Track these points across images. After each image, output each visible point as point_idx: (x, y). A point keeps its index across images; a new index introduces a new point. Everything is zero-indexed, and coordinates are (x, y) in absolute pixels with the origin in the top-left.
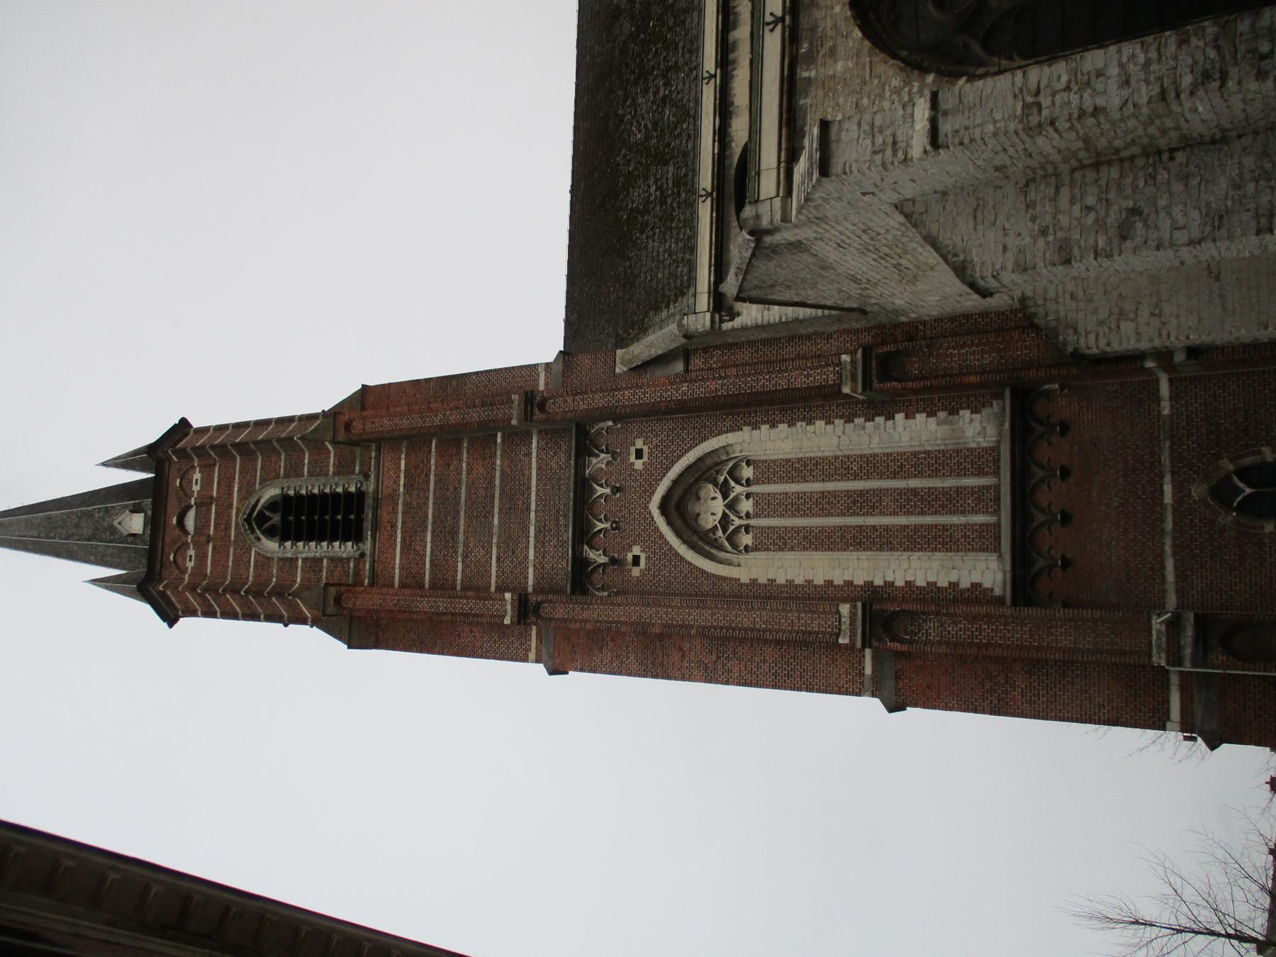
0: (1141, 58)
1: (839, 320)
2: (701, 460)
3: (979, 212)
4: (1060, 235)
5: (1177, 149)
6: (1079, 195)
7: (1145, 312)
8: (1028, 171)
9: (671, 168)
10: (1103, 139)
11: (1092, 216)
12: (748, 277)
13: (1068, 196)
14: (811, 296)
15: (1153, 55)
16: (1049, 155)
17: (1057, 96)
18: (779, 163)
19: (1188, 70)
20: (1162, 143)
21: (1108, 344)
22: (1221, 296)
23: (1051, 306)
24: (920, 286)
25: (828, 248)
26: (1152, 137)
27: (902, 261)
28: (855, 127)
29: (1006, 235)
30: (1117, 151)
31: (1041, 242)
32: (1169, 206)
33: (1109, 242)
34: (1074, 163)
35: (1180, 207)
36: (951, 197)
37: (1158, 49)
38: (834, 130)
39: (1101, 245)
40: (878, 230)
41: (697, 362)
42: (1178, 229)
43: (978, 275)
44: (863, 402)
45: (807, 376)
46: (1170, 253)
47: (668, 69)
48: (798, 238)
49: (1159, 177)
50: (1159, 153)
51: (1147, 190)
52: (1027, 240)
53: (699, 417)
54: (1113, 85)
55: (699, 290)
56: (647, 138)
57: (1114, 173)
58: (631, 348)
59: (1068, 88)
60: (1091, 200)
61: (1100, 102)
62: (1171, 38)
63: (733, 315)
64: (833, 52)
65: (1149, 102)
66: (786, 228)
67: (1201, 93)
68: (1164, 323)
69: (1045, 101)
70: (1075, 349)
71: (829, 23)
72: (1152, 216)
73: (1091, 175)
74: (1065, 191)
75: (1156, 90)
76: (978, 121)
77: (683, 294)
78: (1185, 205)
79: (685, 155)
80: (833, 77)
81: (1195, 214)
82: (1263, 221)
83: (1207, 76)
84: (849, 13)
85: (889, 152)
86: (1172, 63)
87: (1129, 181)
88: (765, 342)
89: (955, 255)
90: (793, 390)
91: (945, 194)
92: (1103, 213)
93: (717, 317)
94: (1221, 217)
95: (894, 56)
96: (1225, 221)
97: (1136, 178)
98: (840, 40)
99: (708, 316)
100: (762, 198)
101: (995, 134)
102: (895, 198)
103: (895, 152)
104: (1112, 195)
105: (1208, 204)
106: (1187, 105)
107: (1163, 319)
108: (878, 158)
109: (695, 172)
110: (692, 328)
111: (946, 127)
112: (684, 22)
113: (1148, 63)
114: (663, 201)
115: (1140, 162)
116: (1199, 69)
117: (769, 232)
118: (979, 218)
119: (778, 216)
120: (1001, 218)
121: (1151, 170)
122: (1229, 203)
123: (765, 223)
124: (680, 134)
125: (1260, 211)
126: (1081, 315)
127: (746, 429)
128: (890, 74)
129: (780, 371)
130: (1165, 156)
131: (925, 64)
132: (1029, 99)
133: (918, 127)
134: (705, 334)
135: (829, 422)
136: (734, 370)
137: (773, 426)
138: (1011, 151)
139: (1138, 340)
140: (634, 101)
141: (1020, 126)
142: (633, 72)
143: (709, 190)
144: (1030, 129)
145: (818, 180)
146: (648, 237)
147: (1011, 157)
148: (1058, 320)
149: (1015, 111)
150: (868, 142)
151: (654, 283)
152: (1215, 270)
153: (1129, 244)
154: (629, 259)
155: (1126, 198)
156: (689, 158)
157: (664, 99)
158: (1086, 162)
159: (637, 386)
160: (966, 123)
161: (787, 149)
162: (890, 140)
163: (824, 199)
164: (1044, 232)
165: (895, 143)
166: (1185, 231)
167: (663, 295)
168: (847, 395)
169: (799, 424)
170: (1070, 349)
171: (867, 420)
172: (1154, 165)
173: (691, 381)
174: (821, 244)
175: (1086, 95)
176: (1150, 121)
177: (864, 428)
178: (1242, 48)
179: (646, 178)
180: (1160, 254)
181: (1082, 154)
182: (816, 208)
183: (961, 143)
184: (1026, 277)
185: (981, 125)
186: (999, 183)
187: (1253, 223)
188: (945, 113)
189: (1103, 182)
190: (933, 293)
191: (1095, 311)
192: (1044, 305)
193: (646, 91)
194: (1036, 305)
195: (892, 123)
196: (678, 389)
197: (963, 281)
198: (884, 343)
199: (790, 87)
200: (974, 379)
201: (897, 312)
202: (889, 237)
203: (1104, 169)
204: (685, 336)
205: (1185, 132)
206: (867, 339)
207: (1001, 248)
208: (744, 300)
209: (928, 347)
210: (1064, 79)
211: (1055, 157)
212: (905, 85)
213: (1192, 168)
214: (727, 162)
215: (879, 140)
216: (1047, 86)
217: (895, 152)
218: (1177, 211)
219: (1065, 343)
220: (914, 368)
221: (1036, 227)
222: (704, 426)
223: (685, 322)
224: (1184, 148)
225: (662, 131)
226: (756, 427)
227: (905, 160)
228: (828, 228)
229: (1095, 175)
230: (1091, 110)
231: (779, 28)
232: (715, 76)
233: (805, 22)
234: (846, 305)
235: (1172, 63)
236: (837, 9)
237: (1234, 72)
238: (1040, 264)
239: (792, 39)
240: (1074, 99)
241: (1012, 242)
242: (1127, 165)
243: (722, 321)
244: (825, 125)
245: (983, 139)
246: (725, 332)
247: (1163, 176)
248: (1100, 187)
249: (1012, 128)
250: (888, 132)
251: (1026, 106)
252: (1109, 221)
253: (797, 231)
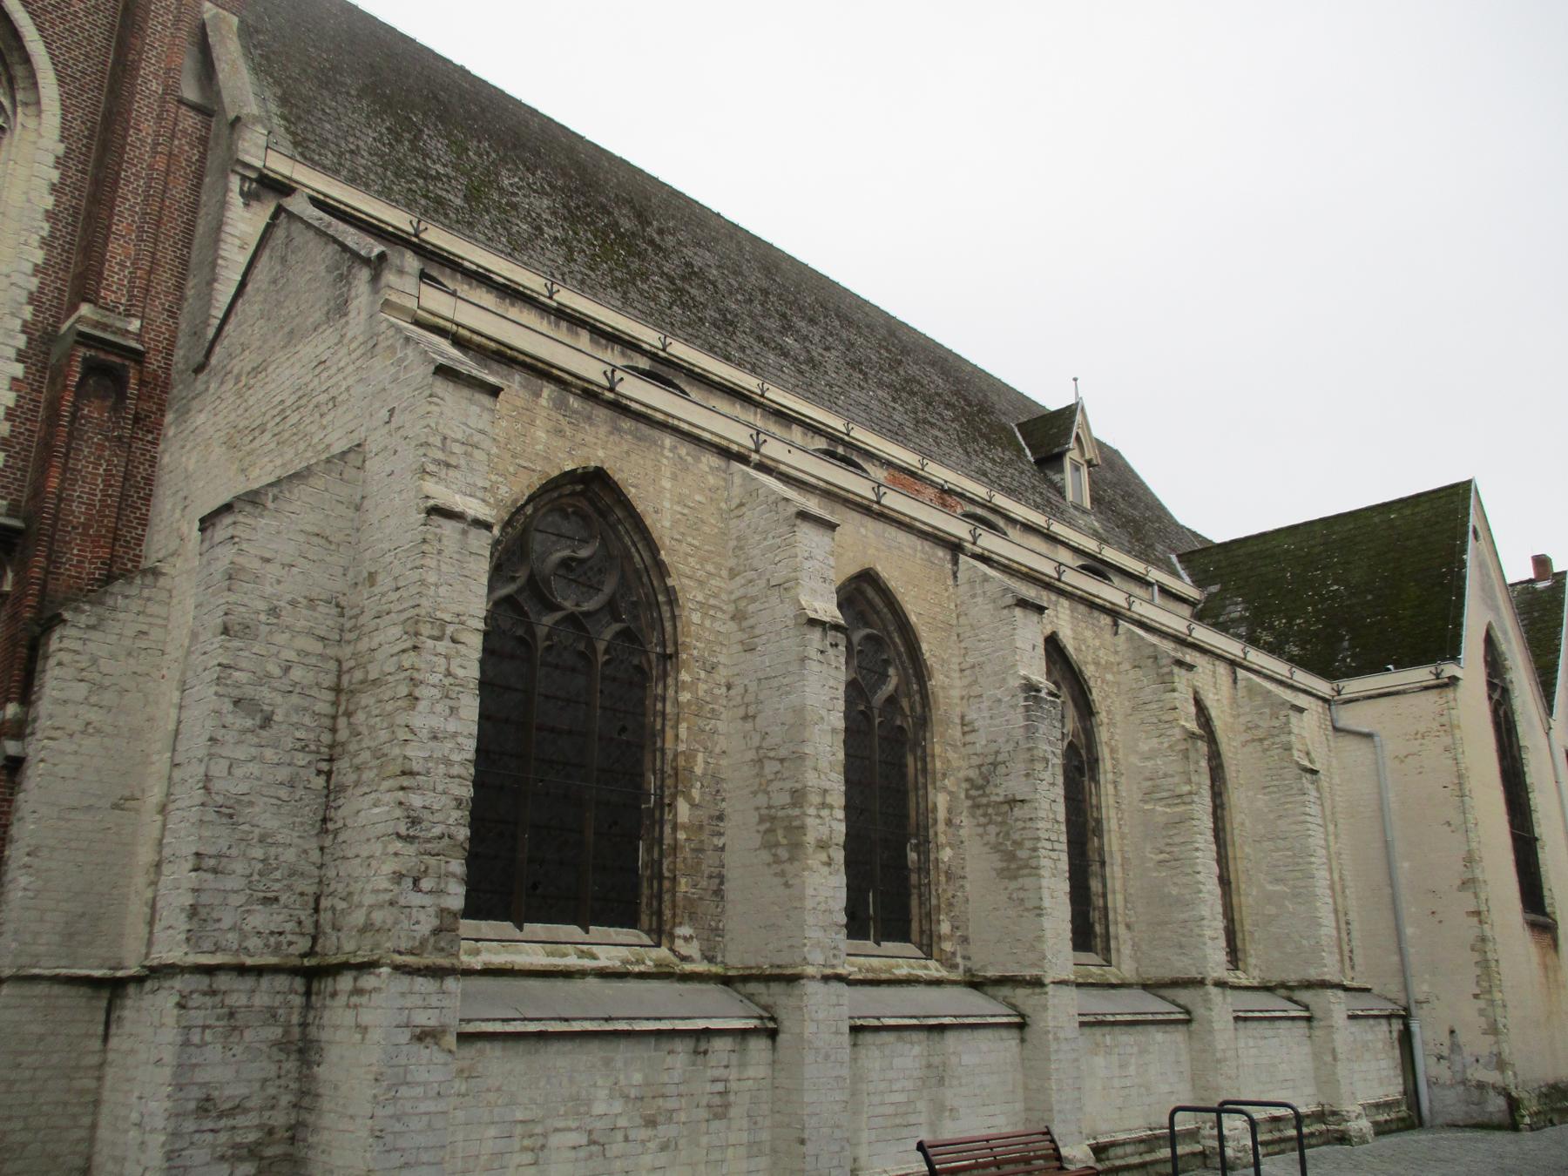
0: (456, 757)
1: (196, 334)
2: (26, 59)
3: (322, 542)
4: (264, 629)
5: (328, 781)
6: (307, 661)
7: (94, 715)
8: (356, 611)
9: (458, 202)
10: (372, 701)
11: (277, 672)
12: (311, 234)
13: (310, 649)
14: (249, 308)
15: (456, 770)
16: (371, 638)
17: (443, 661)
18: (458, 325)
19: (427, 804)
20: (343, 765)
21: (60, 664)
22: (90, 807)
23: (135, 606)
24: (218, 450)
25: (322, 347)
26: (356, 755)
27: (267, 436)
28: (481, 426)
29: (283, 565)
30: (348, 714)
31: (262, 605)
32: (262, 760)
33: (238, 685)
34: (346, 666)
35: (257, 773)
36: (350, 513)
37: (459, 777)
38: (486, 400)
39: (237, 674)
40: (329, 417)
41: (189, 121)
42: (230, 767)
43: (240, 518)
44: (56, 328)
45: (122, 264)
46: (201, 753)
47: (571, 250)
48: (353, 314)
49: (301, 755)
50: (331, 760)
51: (290, 739)
52: (268, 590)
53: (100, 88)
54: (436, 722)
55: (299, 167)
56: (501, 189)
57: (323, 707)
58: (235, 39)
59: (448, 674)
60: (297, 674)
61: (422, 706)
62: (467, 792)
63: (249, 197)
64: (559, 432)
65: (405, 757)
66: (374, 303)
67: (398, 813)
68: (71, 736)
69: (442, 646)
70: (64, 621)
71: (590, 439)
72: (256, 740)
73: (329, 680)
74: (318, 647)
75: (416, 767)
76: (444, 568)
77: (296, 144)
78: (258, 779)
79: (470, 225)
80: (532, 423)
81: (243, 788)
82: (212, 862)
83: (414, 822)
84: (593, 464)
85: (440, 456)
86: (440, 788)
87: (307, 720)
88: (190, 228)
89: (275, 498)
90: (107, 238)
91: (358, 508)
92: (276, 684)
93: (253, 175)
94: (231, 816)
95: (531, 499)
96: (224, 820)
97: (308, 729)
98: (568, 444)
99: (259, 164)
100: (423, 286)
101: (423, 582)
102: (372, 447)
103: (438, 462)
104: (295, 699)
105: (251, 804)
106: (387, 797)
107: (78, 736)
108: (437, 441)
109: (449, 228)
110: (248, 135)
111: (449, 528)
112: (614, 287)
113: (448, 762)
114: (421, 173)
115: (326, 738)
116: (426, 815)
117: (375, 279)
118: (315, 540)
119: (394, 298)
120: (308, 566)
121: (313, 747)
122: (246, 827)
123: (390, 277)
124: (495, 230)
125: (225, 860)
126: (112, 638)
127: (61, 149)
128: (517, 488)
129: (140, 229)
130: (324, 766)
131: (509, 530)
132: (449, 630)
133: (458, 497)
134: (231, 147)
135: (37, 270)
136: (162, 166)
137: (54, 189)
138: (394, 596)
139: (56, 701)
140: (547, 194)
141: (423, 612)
142: (578, 208)
143: (423, 236)
144: (417, 622)
145: (434, 360)
146: (381, 135)
147: (383, 595)
148: (114, 609)
149: (443, 611)
150: (459, 436)
151: (320, 114)
152: (128, 804)
153: (227, 706)
154: (359, 98)
155: (287, 715)
156: (465, 226)
157: (539, 228)
158: (345, 679)
159: (178, 20)
160: (446, 553)
161: (470, 341)
162: (453, 461)
163: (402, 360)
164: (274, 611)
165: (448, 465)
166: (225, 773)
167: (299, 118)
168: (74, 307)
169: (46, 226)
170: (67, 615)
171: (25, 324)
172: (318, 752)
173: (163, 101)
174: (334, 339)
175: (434, 691)
176: (378, 754)
177: (13, 314)
178: (432, 861)
179: (455, 167)
180: (202, 740)
181: (358, 675)
182: (392, 348)
183: (424, 541)
184: (218, 576)
185: (439, 569)
186: (351, 574)
187: (212, 851)
188: (464, 532)
189: (314, 692)
190: (199, 458)
191: (113, 657)
192: (140, 597)
193: (554, 213)
194: (143, 586)
195: (472, 470)
196: (156, 76)
197: (238, 498)
198: (142, 383)
199: (540, 371)
200: (54, 482)
201: (184, 413)
202: (313, 428)
203: (330, 696)
204: (238, 119)
205: (350, 791)
206: (154, 362)
207: (268, 555)
208: (275, 216)
209: (120, 438)
210: (460, 673)
211: (363, 645)
212: (496, 500)
213: (300, 792)
214: (448, 271)
215: (457, 448)
216: (458, 652)
217: (438, 462)
218: (254, 768)
219: (77, 610)
220: (94, 411)
221: (282, 604)
222: (82, 89)
223: (260, 129)
224: (327, 787)
225: (505, 212)
226: (59, 163)
227: (424, 471)
228: (354, 356)
229: (326, 685)
230: (417, 693)
231: (605, 383)
232: (550, 298)
233: (601, 413)
234: (217, 349)
235: (440, 788)
236: (601, 453)
237: (411, 849)
238: (232, 598)
239: (590, 394)
240: (435, 679)
241: (273, 570)
242: (327, 722)
243: (244, 178)
244: (494, 391)
245: (422, 567)
246: (226, 177)
247: (301, 759)
248: (310, 687)
249: (424, 602)
250: (462, 462)
251: (444, 624)
252: (265, 690)
253: (364, 316)
